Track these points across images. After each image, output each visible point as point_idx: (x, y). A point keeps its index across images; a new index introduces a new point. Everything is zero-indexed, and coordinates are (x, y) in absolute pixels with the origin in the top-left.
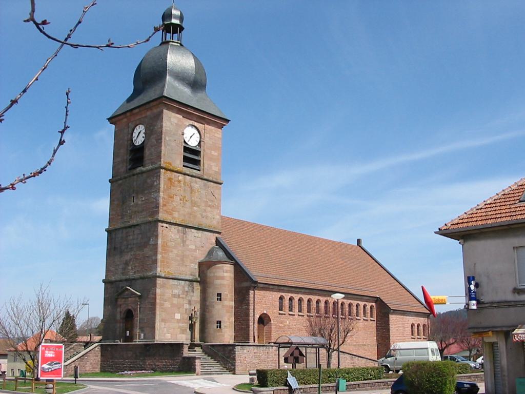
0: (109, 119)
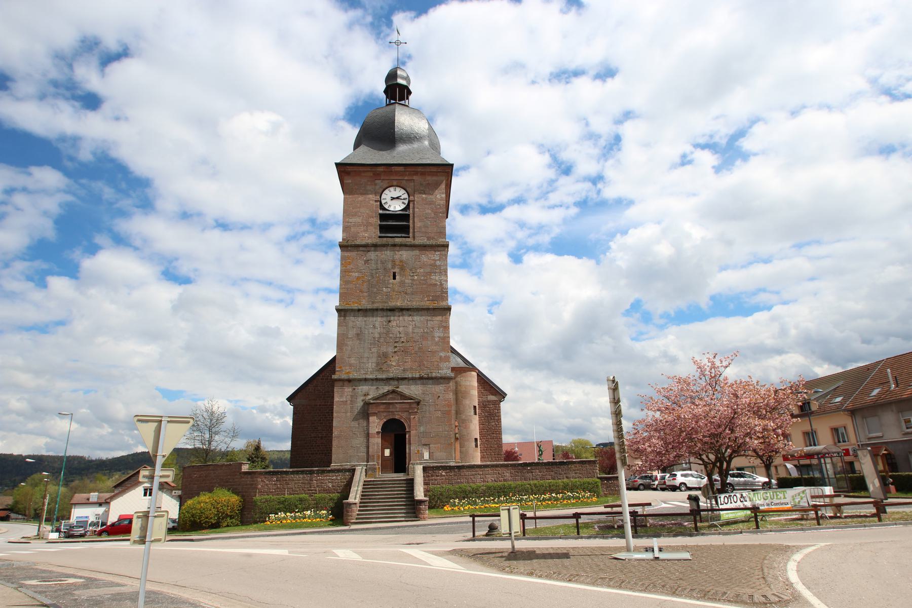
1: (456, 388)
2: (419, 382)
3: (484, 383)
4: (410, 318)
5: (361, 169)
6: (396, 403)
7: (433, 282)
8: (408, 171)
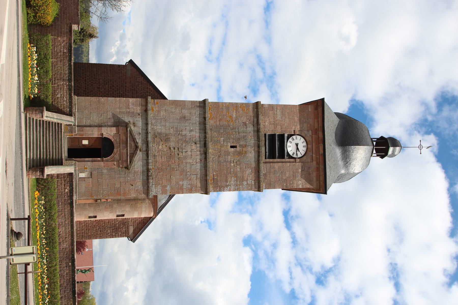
1: (140, 199)
3: (144, 223)
4: (198, 160)
5: (320, 119)
6: (127, 150)
8: (319, 156)
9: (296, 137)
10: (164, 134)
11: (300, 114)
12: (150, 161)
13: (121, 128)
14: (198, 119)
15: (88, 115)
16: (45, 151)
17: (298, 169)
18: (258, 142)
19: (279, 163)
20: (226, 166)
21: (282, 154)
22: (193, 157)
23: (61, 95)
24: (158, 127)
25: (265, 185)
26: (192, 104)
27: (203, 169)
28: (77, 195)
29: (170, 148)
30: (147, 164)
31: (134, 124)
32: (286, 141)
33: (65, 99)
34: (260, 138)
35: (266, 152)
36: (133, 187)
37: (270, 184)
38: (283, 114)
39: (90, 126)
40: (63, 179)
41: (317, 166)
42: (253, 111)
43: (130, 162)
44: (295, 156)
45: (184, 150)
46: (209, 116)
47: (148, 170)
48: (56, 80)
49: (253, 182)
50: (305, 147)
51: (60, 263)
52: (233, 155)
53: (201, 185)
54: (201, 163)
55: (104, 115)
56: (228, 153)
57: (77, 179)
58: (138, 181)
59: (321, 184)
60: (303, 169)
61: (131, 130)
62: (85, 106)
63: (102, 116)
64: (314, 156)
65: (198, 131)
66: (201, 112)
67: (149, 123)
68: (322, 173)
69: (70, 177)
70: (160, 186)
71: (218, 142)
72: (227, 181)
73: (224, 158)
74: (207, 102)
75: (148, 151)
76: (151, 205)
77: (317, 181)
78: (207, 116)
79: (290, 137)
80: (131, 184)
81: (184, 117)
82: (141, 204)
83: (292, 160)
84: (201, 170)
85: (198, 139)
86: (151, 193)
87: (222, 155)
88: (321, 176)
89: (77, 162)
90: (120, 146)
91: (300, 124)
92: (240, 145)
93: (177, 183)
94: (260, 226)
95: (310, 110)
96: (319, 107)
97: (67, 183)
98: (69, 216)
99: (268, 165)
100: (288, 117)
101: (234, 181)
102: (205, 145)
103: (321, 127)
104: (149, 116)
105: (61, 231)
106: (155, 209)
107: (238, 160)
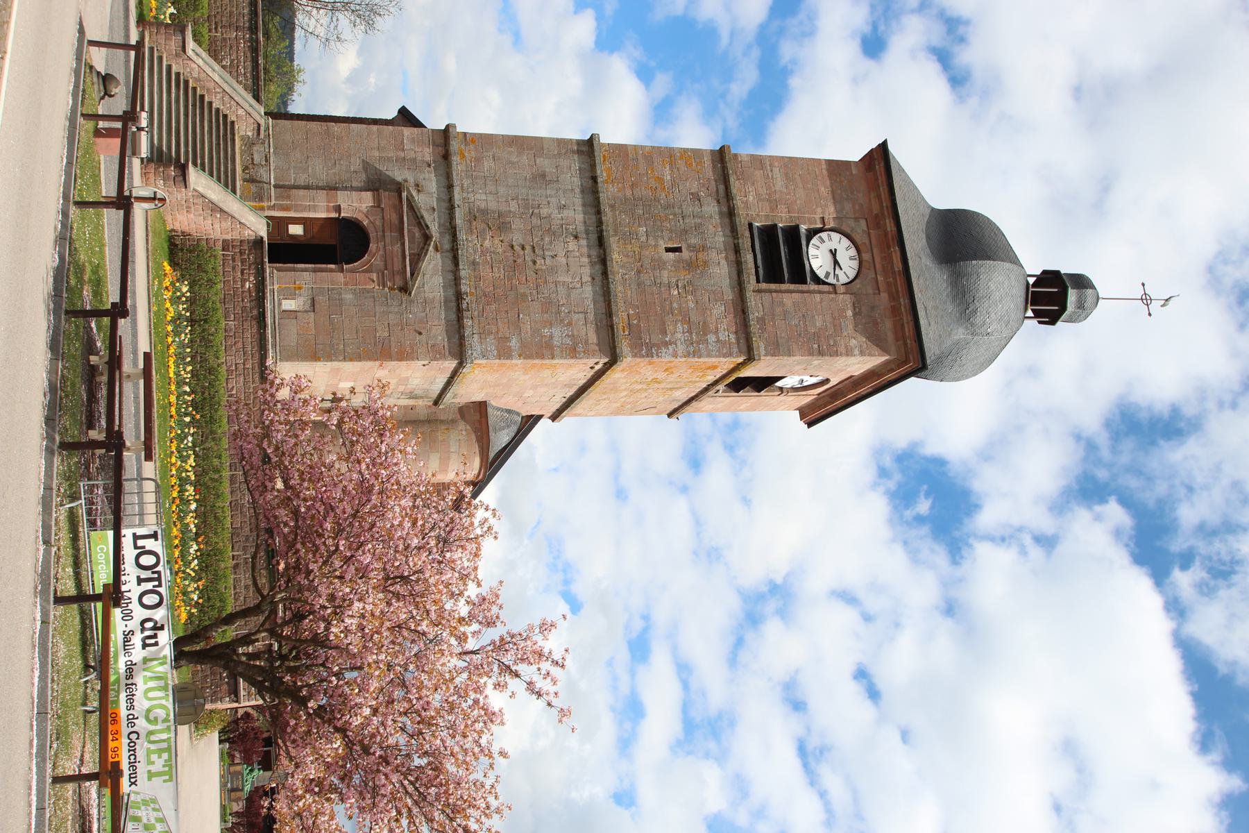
0: (883, 147)
1: (442, 422)
2: (451, 292)
4: (587, 278)
5: (883, 190)
6: (403, 244)
7: (670, 328)
8: (895, 279)
9: (829, 236)
10: (494, 212)
11: (830, 179)
12: (463, 273)
13: (384, 195)
14: (577, 181)
15: (301, 162)
16: (190, 150)
17: (842, 311)
18: (734, 239)
19: (793, 294)
20: (660, 293)
21: (799, 273)
22: (572, 269)
23: (232, 61)
24: (478, 196)
25: (763, 346)
26: (559, 146)
27: (602, 299)
28: (278, 354)
29: (512, 247)
30: (457, 280)
31: (417, 185)
32: (804, 242)
33: (242, 70)
34: (739, 229)
35: (756, 267)
36: (423, 337)
37: (778, 345)
38: (788, 178)
39: (307, 187)
40: (238, 257)
41: (892, 304)
42: (714, 167)
43: (412, 275)
44: (831, 280)
45: (547, 253)
46: (605, 175)
47: (459, 296)
48: (219, 28)
49: (732, 337)
50: (855, 259)
51: (231, 471)
52: (673, 269)
53: (598, 338)
54: (593, 285)
55: (342, 162)
56: (659, 265)
57: (276, 312)
58: (436, 323)
59: (909, 346)
60: (857, 310)
61: (410, 198)
62: (293, 142)
63: (337, 165)
64: (880, 278)
65: (581, 209)
66: (582, 166)
67: (456, 182)
68: (907, 318)
69: (258, 251)
70: (492, 337)
71: (632, 235)
72: (664, 332)
73: (651, 275)
74: (595, 143)
75: (457, 249)
76: (473, 436)
77: (897, 341)
78: (599, 172)
79: (815, 235)
80: (416, 331)
81: (543, 176)
82: (446, 431)
83: (825, 288)
84: (595, 302)
85: (581, 228)
86: (470, 352)
87: (646, 269)
88: (906, 325)
89: (275, 271)
90: (384, 236)
91: (834, 203)
92: (689, 246)
93: (536, 331)
94: (740, 787)
95: (854, 172)
96: (877, 163)
97: (250, 266)
98: (256, 348)
99: (766, 296)
100: (801, 186)
101: (683, 333)
102: (601, 242)
103: (887, 207)
104: (454, 167)
105: (233, 387)
106: (485, 446)
107: (688, 282)
